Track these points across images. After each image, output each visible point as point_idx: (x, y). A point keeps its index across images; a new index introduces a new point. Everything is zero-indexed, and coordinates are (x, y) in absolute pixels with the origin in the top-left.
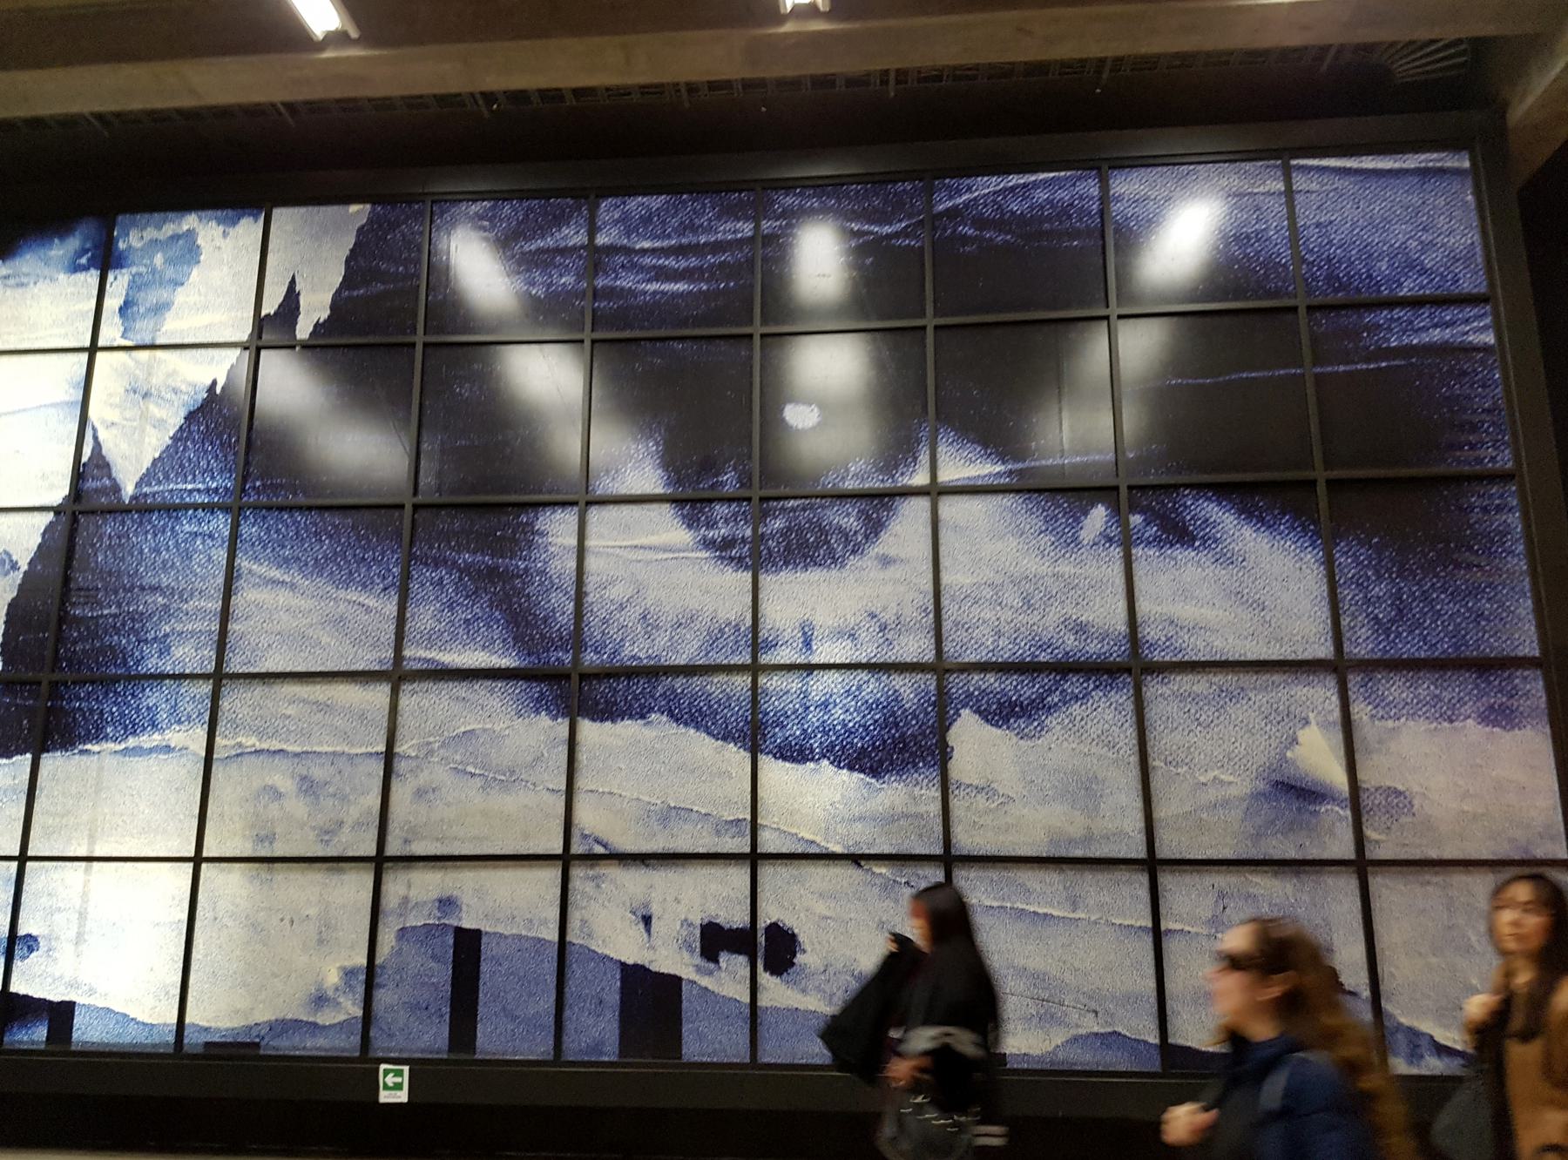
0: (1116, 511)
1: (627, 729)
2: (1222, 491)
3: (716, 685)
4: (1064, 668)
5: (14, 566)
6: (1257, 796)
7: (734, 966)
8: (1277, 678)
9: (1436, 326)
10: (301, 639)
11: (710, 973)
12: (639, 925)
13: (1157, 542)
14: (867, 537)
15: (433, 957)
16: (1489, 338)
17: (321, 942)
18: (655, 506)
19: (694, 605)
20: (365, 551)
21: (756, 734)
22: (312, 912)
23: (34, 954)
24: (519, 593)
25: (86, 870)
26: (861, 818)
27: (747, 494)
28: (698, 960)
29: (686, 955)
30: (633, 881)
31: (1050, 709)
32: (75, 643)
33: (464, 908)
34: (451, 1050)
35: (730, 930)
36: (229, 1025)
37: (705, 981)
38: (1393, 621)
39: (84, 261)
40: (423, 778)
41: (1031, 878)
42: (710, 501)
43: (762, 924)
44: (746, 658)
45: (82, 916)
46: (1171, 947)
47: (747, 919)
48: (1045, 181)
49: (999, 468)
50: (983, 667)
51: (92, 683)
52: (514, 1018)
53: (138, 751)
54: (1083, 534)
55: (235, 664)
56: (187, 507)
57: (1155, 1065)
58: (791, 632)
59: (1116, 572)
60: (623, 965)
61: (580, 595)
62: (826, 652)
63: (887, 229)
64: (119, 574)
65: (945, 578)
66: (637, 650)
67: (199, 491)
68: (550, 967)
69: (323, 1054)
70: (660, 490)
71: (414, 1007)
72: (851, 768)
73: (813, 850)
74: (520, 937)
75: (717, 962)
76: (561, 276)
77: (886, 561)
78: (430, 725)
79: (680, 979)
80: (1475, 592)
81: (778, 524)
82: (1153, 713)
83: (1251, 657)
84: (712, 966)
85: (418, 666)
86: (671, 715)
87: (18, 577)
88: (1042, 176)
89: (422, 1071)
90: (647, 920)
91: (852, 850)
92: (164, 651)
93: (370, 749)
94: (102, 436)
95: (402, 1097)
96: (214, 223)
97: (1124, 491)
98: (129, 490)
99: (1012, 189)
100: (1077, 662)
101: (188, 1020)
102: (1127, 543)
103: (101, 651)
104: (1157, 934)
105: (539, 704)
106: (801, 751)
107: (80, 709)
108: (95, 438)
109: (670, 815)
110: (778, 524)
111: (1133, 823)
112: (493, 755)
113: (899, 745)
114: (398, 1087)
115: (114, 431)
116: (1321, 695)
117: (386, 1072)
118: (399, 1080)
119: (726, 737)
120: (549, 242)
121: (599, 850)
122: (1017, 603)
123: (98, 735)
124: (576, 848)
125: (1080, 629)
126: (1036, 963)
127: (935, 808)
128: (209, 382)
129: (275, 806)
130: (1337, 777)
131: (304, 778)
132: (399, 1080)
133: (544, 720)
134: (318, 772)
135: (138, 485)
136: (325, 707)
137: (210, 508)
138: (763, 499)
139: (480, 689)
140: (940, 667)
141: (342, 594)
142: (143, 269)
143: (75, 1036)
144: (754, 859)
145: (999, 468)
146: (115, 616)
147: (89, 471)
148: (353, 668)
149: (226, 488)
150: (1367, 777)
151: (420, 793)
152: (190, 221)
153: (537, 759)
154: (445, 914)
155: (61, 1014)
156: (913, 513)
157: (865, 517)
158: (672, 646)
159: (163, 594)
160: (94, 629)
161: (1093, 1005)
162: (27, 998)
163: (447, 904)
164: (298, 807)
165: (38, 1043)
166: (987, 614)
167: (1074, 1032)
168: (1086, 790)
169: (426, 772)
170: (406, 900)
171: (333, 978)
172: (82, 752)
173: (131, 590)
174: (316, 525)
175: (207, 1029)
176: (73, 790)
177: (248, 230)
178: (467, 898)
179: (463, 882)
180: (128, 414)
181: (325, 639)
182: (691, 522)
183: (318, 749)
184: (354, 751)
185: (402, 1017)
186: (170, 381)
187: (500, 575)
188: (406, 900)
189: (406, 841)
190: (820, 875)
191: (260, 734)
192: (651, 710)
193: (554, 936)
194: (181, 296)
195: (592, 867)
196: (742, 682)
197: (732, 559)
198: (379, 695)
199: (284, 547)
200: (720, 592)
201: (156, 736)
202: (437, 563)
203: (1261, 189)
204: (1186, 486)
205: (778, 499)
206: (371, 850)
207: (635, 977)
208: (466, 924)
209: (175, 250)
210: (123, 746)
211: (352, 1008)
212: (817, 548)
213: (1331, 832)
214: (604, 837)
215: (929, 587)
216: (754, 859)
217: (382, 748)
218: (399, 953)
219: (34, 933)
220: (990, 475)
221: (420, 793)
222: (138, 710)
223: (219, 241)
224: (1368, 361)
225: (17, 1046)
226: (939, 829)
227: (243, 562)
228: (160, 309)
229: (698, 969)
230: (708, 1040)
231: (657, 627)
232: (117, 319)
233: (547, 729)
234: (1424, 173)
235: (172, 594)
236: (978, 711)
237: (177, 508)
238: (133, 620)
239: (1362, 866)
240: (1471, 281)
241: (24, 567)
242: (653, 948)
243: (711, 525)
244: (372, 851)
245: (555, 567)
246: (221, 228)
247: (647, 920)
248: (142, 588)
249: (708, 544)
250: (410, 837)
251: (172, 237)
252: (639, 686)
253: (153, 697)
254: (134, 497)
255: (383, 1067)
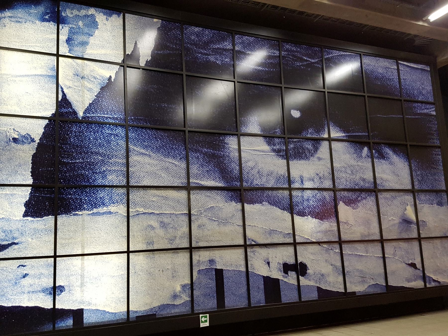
0: (370, 149)
1: (257, 206)
2: (391, 146)
3: (280, 194)
4: (361, 190)
5: (33, 140)
6: (400, 223)
7: (292, 275)
8: (402, 194)
9: (425, 109)
10: (154, 175)
11: (286, 277)
12: (267, 264)
13: (378, 158)
14: (314, 151)
15: (210, 279)
16: (434, 113)
17: (173, 277)
18: (258, 138)
19: (272, 169)
20: (173, 145)
21: (291, 208)
22: (169, 267)
23: (63, 293)
24: (222, 162)
25: (82, 259)
26: (319, 232)
27: (284, 136)
28: (283, 274)
29: (280, 272)
30: (263, 252)
31: (359, 201)
32: (65, 173)
33: (217, 262)
34: (217, 308)
35: (290, 265)
36: (144, 309)
37: (285, 280)
38: (421, 180)
39: (47, 17)
40: (200, 221)
41: (357, 246)
42: (274, 137)
43: (299, 262)
44: (286, 186)
45: (82, 276)
46: (387, 261)
47: (294, 261)
48: (349, 55)
49: (343, 135)
50: (344, 190)
51: (75, 188)
52: (235, 295)
53: (98, 214)
54: (363, 154)
55: (132, 183)
56: (106, 124)
57: (384, 291)
58: (298, 179)
59: (370, 165)
60: (264, 276)
61: (240, 165)
62: (307, 185)
63: (313, 61)
64: (81, 147)
65: (334, 165)
66: (258, 182)
67: (110, 118)
68: (244, 279)
69: (178, 314)
70: (259, 133)
71: (205, 295)
72: (316, 218)
73: (309, 241)
74: (234, 270)
75: (288, 274)
76: (225, 58)
77: (319, 159)
78: (200, 205)
79: (279, 279)
80: (435, 174)
81: (292, 146)
82: (381, 202)
83: (397, 188)
84: (287, 275)
85: (194, 185)
86: (269, 202)
87: (35, 145)
88: (348, 53)
89: (213, 315)
90: (268, 263)
91: (318, 241)
92: (104, 177)
93: (182, 212)
94: (66, 91)
95: (207, 324)
96: (102, 14)
97: (372, 144)
98: (81, 114)
99: (342, 55)
100: (364, 189)
101: (130, 309)
102: (372, 158)
103: (78, 176)
104: (384, 258)
105: (232, 199)
106: (303, 213)
107: (71, 198)
108: (63, 92)
109: (272, 232)
110: (292, 146)
111: (377, 231)
112: (220, 215)
113: (327, 211)
114: (206, 321)
115: (70, 90)
116: (409, 198)
117: (202, 317)
118: (206, 319)
119: (284, 209)
120: (220, 46)
121: (253, 243)
122: (350, 173)
123: (80, 208)
124: (248, 243)
125: (364, 180)
126: (360, 268)
127: (336, 228)
128: (108, 77)
129: (152, 232)
130: (414, 218)
131: (161, 222)
132: (206, 319)
133: (234, 203)
134: (166, 220)
135: (84, 113)
136: (166, 198)
137: (116, 125)
138: (288, 138)
139: (213, 194)
140: (334, 190)
141: (167, 160)
142: (74, 26)
143: (85, 321)
144: (295, 244)
145: (343, 135)
146: (82, 163)
147: (63, 103)
148: (173, 185)
149: (121, 118)
150: (420, 219)
151: (199, 226)
152: (92, 11)
153: (233, 215)
154: (212, 265)
155: (78, 314)
156: (325, 144)
157: (313, 145)
158: (267, 181)
159: (101, 155)
160: (73, 167)
161: (372, 277)
162: (62, 310)
163: (212, 261)
164: (160, 232)
165: (69, 326)
166: (344, 175)
167: (369, 284)
168: (367, 223)
169: (201, 220)
170: (199, 261)
171: (178, 288)
172: (74, 215)
173: (87, 153)
174: (155, 135)
175: (136, 312)
176: (72, 229)
177: (116, 20)
178: (217, 259)
179: (216, 254)
180: (76, 84)
181: (163, 175)
182: (269, 144)
183: (165, 212)
184: (177, 213)
185: (202, 299)
186: (92, 74)
187: (216, 156)
188: (199, 261)
189: (197, 242)
190: (311, 248)
191: (144, 207)
192: (263, 201)
193: (243, 269)
194: (92, 40)
195: (252, 248)
196: (286, 193)
197: (280, 155)
198: (183, 195)
199: (145, 142)
200: (278, 165)
201: (105, 208)
202: (196, 151)
203: (392, 67)
204: (383, 144)
205: (291, 138)
206: (187, 245)
207: (267, 280)
208: (218, 268)
209: (87, 21)
210: (92, 212)
211: (186, 298)
212: (302, 154)
213: (413, 232)
214: (254, 239)
215: (330, 167)
216: (295, 244)
217: (186, 212)
218: (199, 278)
219: (62, 285)
220: (342, 136)
221: (199, 226)
222: (96, 198)
223: (105, 22)
224: (414, 116)
225: (60, 328)
226: (337, 234)
227: (131, 146)
228: (84, 44)
229: (283, 276)
230: (288, 296)
231: (262, 176)
232: (65, 44)
233: (235, 206)
234: (422, 70)
235: (105, 156)
236: (344, 202)
237: (103, 124)
238: (90, 165)
239: (419, 239)
240: (431, 99)
241: (38, 141)
242: (271, 271)
243: (274, 145)
244: (187, 245)
245: (232, 155)
246: (105, 17)
247: (268, 263)
248: (92, 153)
249: (274, 151)
250: (198, 241)
251: (85, 16)
252: (259, 193)
253: (102, 194)
254: (83, 118)
255: (201, 315)
